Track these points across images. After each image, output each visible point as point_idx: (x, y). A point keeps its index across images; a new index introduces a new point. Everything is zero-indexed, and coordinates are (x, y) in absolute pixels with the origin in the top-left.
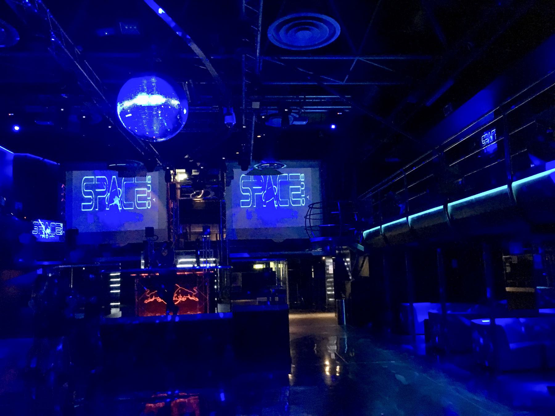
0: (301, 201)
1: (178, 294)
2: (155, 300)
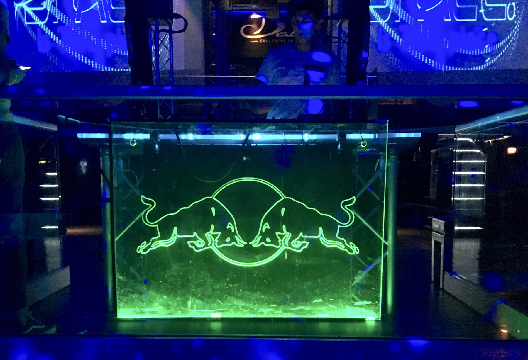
0: (507, 11)
1: (276, 222)
2: (181, 244)
